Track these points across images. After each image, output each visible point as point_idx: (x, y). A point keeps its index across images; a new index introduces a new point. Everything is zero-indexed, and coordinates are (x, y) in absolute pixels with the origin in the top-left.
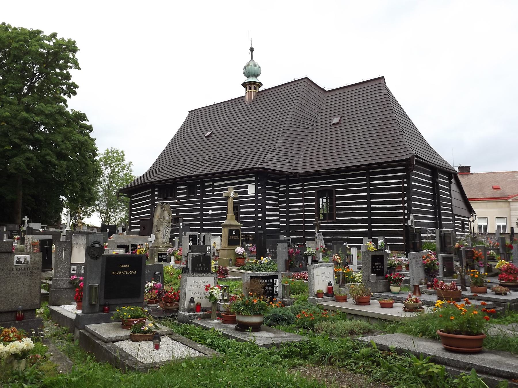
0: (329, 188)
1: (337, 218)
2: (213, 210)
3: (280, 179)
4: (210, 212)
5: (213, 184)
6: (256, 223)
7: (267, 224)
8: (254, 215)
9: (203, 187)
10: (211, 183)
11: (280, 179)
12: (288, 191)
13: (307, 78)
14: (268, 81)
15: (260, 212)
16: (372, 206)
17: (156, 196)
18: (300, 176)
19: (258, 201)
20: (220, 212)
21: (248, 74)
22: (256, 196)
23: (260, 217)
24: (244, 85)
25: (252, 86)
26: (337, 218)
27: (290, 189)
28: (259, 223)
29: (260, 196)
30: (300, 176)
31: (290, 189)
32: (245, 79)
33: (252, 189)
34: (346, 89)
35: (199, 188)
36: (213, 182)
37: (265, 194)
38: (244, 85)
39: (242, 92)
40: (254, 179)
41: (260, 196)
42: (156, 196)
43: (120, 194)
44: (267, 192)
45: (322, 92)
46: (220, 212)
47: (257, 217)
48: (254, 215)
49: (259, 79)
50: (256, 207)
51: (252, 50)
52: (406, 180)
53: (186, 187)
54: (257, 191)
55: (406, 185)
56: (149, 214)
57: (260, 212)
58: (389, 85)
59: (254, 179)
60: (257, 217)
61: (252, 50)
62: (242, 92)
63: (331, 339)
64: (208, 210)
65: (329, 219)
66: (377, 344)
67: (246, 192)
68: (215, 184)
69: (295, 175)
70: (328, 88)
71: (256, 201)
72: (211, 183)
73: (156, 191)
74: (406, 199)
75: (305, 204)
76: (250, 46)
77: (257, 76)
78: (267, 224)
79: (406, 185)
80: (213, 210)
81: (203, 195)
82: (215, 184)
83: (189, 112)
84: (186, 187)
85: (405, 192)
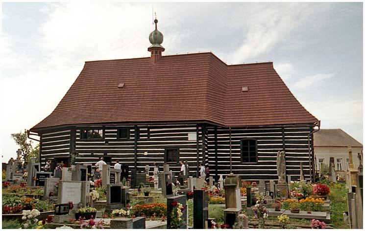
0: (253, 139)
1: (259, 161)
2: (149, 152)
4: (146, 154)
7: (77, 142)
8: (196, 158)
9: (138, 132)
10: (146, 129)
13: (211, 53)
14: (170, 48)
17: (78, 136)
18: (232, 128)
22: (198, 142)
23: (200, 159)
24: (149, 49)
26: (259, 161)
27: (218, 137)
30: (232, 128)
31: (218, 137)
32: (150, 45)
33: (192, 137)
34: (237, 67)
38: (149, 49)
39: (149, 54)
40: (195, 128)
42: (78, 136)
43: (31, 133)
48: (196, 158)
51: (156, 21)
53: (116, 130)
57: (200, 155)
59: (195, 128)
61: (156, 21)
63: (15, 192)
65: (250, 162)
66: (213, 228)
67: (187, 139)
68: (151, 130)
70: (228, 64)
72: (146, 129)
73: (78, 132)
77: (160, 42)
78: (77, 142)
80: (149, 152)
81: (137, 137)
82: (151, 130)
84: (116, 130)
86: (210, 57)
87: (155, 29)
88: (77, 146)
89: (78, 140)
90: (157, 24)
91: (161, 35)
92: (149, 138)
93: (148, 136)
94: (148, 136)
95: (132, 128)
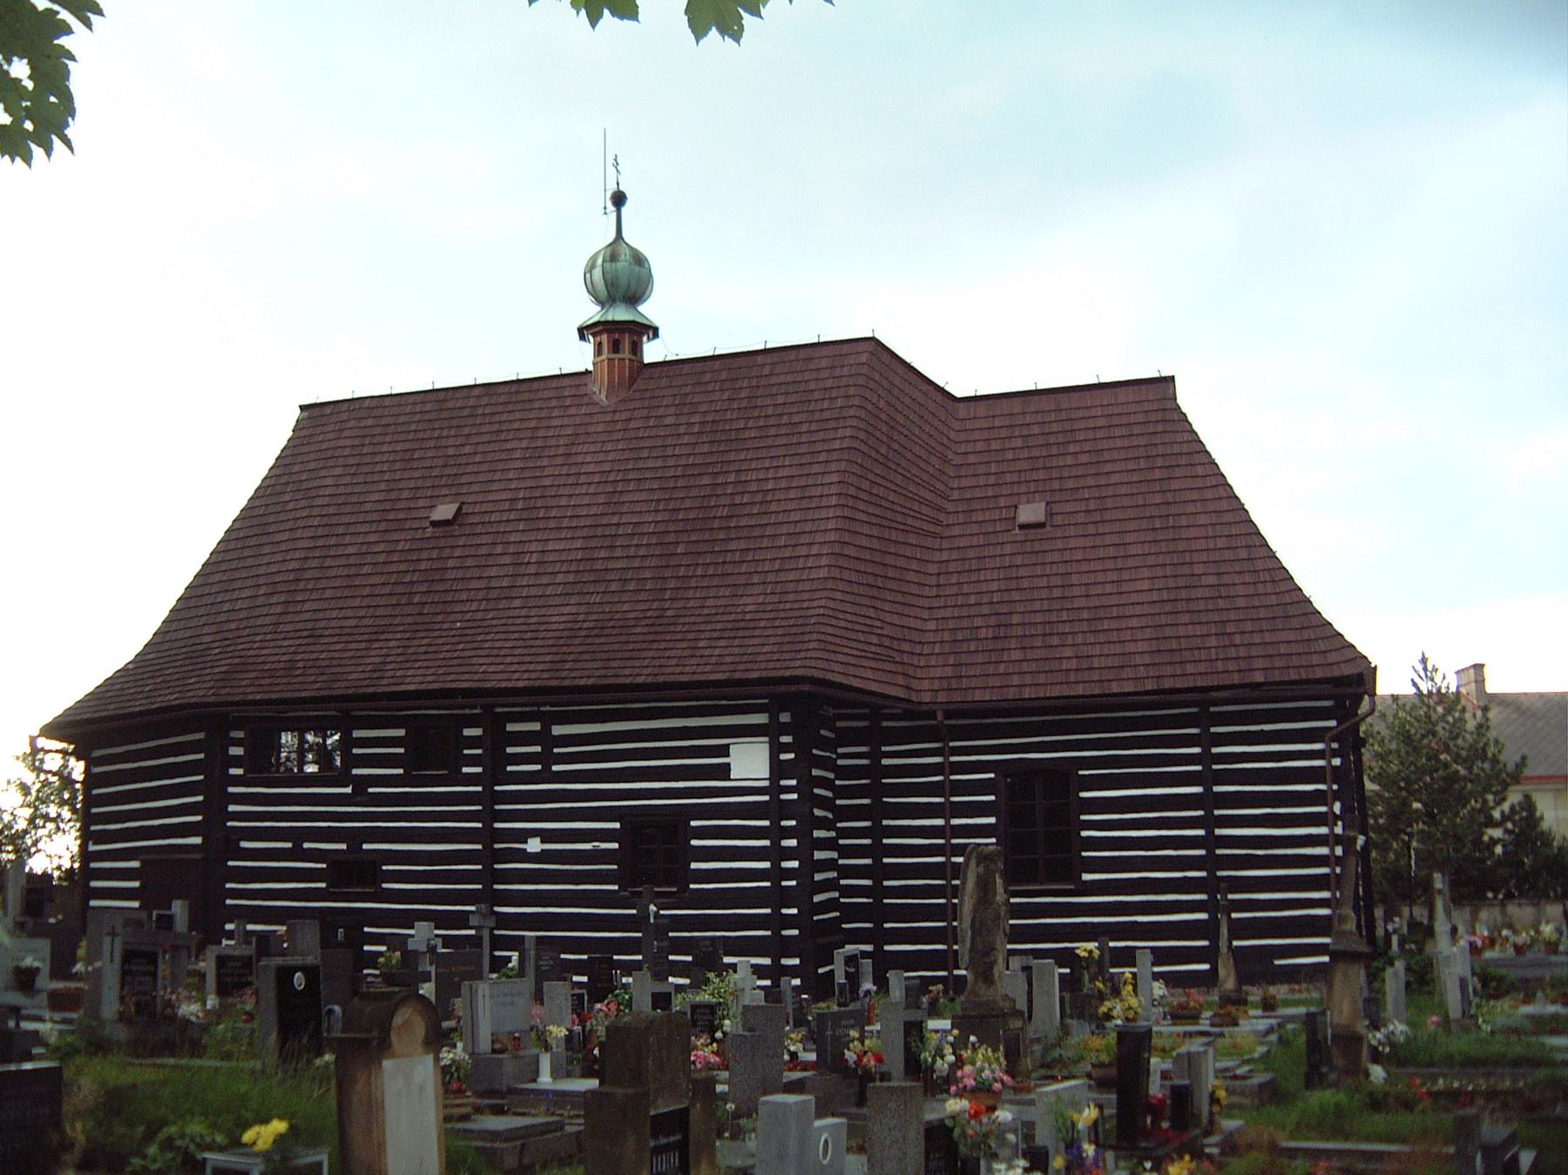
1: (1086, 877)
2: (546, 836)
3: (839, 724)
4: (534, 846)
5: (546, 729)
6: (779, 897)
9: (497, 741)
10: (536, 726)
11: (839, 724)
12: (875, 771)
13: (873, 339)
14: (684, 327)
15: (789, 854)
16: (497, 825)
17: (237, 762)
18: (949, 715)
19: (784, 810)
20: (588, 846)
21: (604, 301)
22: (774, 789)
23: (790, 873)
25: (605, 337)
26: (1086, 877)
27: (885, 762)
28: (785, 897)
29: (789, 790)
30: (949, 715)
31: (885, 762)
32: (591, 312)
33: (749, 763)
35: (473, 742)
36: (549, 720)
37: (807, 783)
39: (581, 357)
40: (761, 719)
41: (789, 790)
44: (815, 772)
45: (939, 398)
46: (588, 846)
47: (777, 874)
49: (649, 310)
50: (777, 833)
52: (1335, 745)
53: (401, 732)
54: (778, 769)
55: (1336, 762)
56: (817, 898)
57: (789, 854)
58: (1186, 399)
59: (761, 719)
60: (777, 874)
61: (619, 199)
62: (581, 357)
64: (524, 835)
67: (724, 772)
68: (557, 730)
69: (912, 711)
70: (959, 394)
71: (774, 809)
72: (536, 726)
74: (1337, 807)
75: (955, 822)
76: (612, 188)
77: (634, 296)
79: (1336, 762)
80: (546, 836)
81: (496, 769)
82: (557, 730)
83: (302, 408)
84: (401, 732)
85: (1335, 787)
86: (869, 366)
87: (612, 236)
88: (232, 808)
89: (237, 781)
90: (623, 210)
91: (639, 260)
92: (547, 768)
93: (546, 758)
94: (546, 758)
95: (472, 722)
